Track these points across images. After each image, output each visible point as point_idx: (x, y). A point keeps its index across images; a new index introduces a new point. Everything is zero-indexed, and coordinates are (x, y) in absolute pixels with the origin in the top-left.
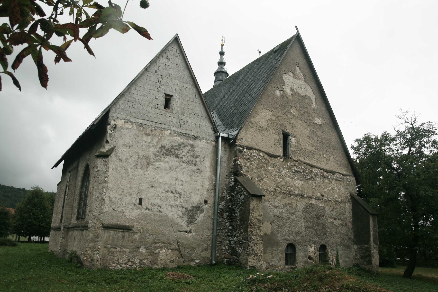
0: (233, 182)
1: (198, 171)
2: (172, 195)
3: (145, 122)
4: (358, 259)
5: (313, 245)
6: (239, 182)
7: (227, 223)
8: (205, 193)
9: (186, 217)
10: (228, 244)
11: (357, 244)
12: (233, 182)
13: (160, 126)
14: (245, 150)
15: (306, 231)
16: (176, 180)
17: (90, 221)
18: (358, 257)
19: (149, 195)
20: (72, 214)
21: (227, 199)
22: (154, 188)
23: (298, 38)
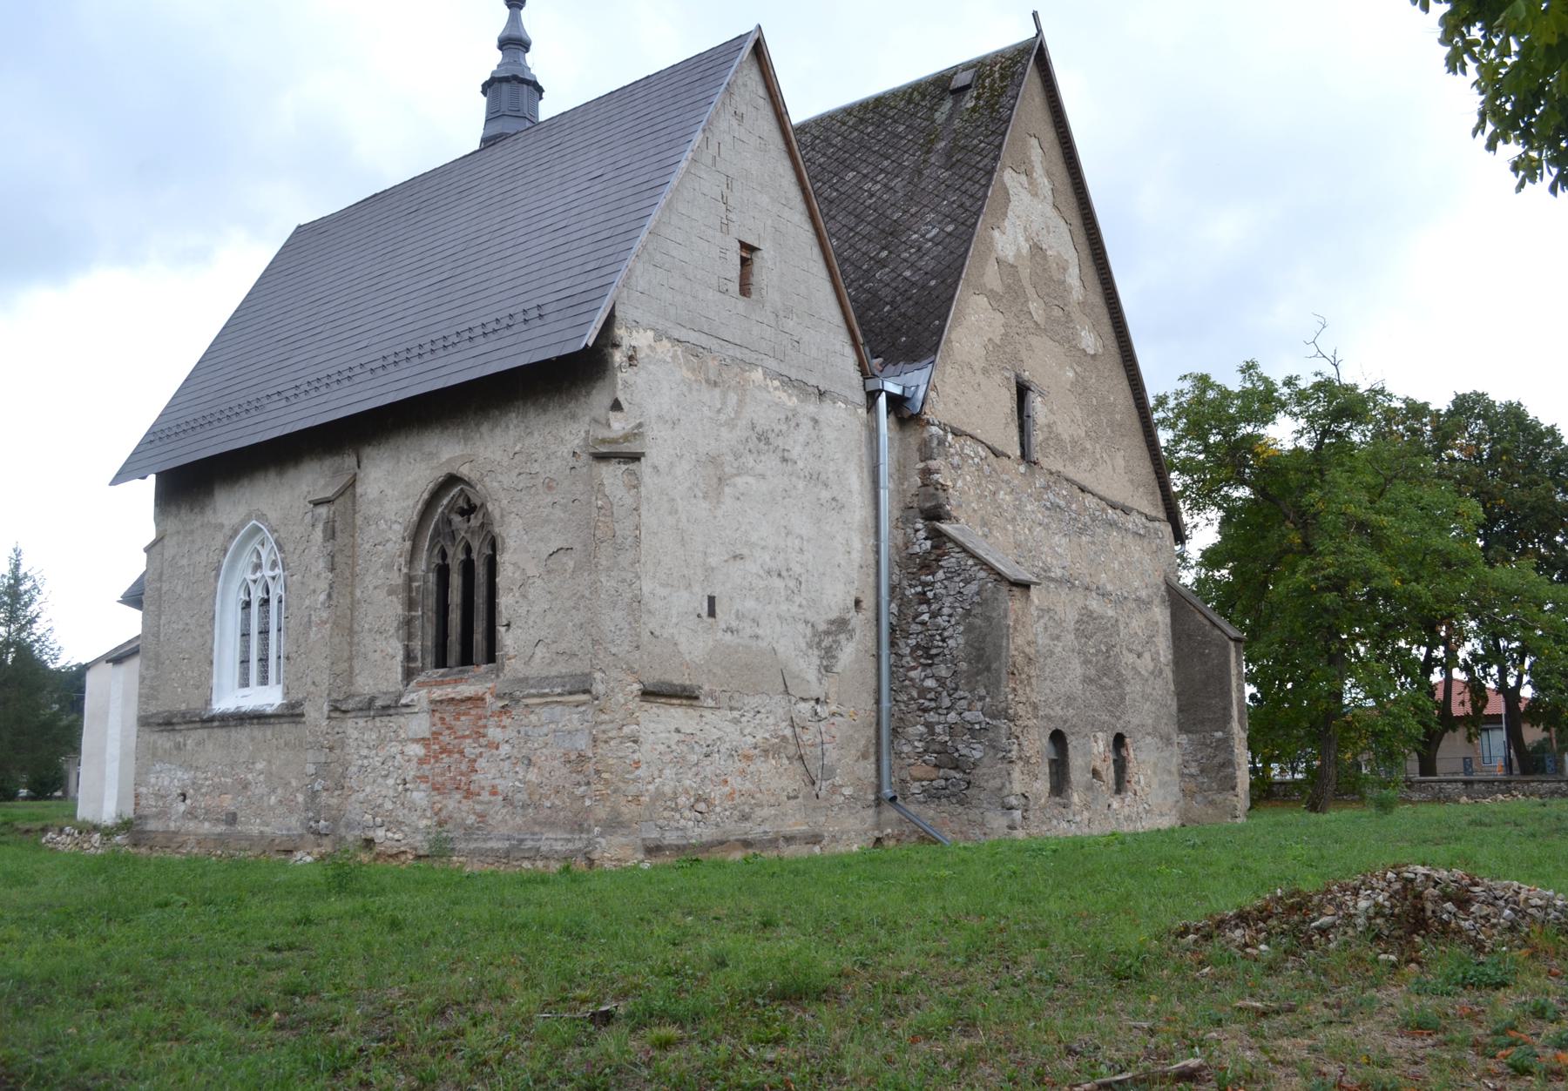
0: (926, 539)
1: (834, 504)
2: (778, 583)
3: (704, 340)
4: (1192, 776)
5: (1099, 735)
6: (951, 539)
7: (914, 668)
8: (855, 575)
9: (816, 652)
10: (921, 735)
11: (1187, 732)
12: (926, 539)
13: (738, 353)
14: (950, 437)
15: (1084, 691)
16: (787, 534)
17: (598, 675)
18: (1194, 770)
19: (729, 585)
20: (351, 659)
21: (907, 593)
22: (739, 562)
23: (1034, 57)
